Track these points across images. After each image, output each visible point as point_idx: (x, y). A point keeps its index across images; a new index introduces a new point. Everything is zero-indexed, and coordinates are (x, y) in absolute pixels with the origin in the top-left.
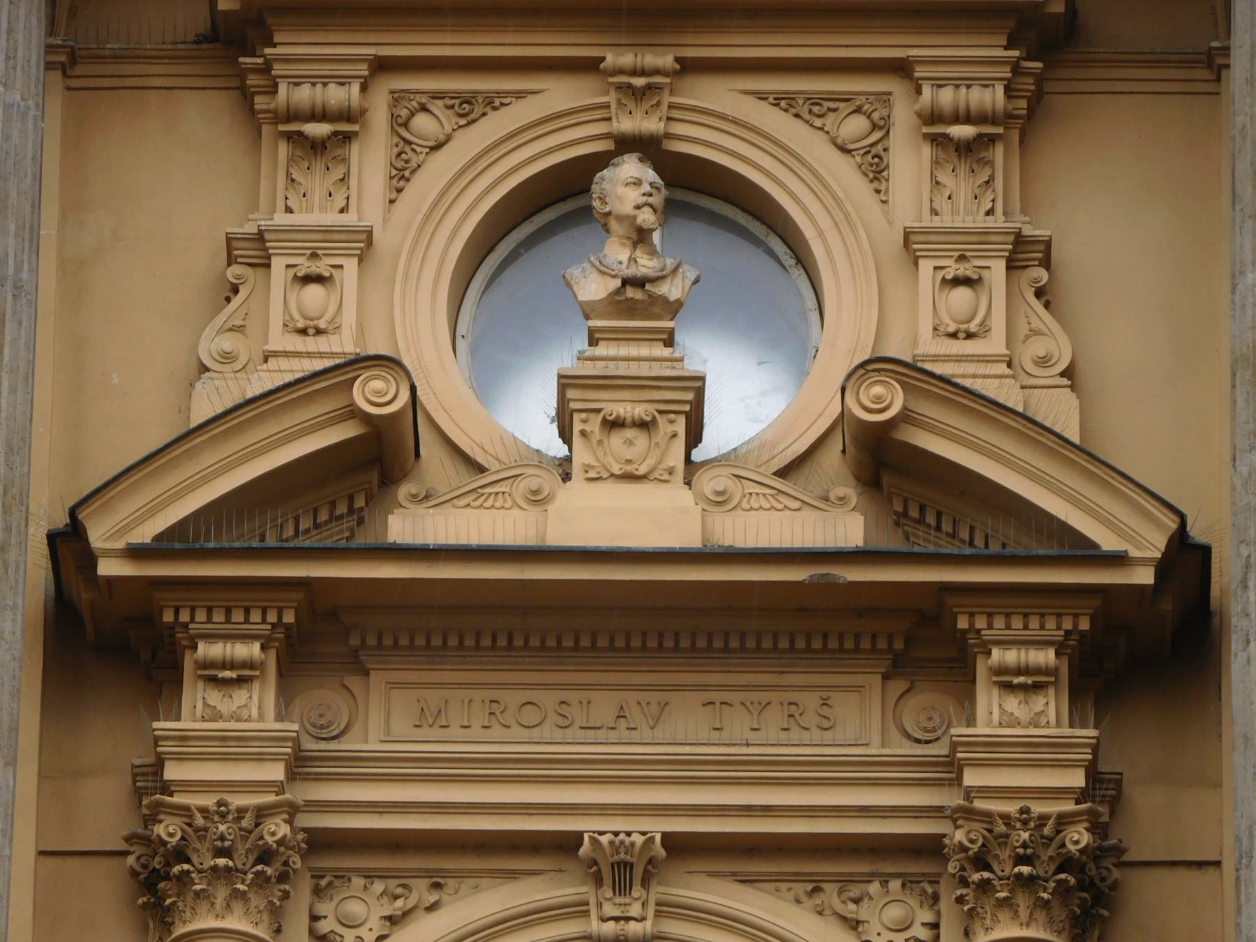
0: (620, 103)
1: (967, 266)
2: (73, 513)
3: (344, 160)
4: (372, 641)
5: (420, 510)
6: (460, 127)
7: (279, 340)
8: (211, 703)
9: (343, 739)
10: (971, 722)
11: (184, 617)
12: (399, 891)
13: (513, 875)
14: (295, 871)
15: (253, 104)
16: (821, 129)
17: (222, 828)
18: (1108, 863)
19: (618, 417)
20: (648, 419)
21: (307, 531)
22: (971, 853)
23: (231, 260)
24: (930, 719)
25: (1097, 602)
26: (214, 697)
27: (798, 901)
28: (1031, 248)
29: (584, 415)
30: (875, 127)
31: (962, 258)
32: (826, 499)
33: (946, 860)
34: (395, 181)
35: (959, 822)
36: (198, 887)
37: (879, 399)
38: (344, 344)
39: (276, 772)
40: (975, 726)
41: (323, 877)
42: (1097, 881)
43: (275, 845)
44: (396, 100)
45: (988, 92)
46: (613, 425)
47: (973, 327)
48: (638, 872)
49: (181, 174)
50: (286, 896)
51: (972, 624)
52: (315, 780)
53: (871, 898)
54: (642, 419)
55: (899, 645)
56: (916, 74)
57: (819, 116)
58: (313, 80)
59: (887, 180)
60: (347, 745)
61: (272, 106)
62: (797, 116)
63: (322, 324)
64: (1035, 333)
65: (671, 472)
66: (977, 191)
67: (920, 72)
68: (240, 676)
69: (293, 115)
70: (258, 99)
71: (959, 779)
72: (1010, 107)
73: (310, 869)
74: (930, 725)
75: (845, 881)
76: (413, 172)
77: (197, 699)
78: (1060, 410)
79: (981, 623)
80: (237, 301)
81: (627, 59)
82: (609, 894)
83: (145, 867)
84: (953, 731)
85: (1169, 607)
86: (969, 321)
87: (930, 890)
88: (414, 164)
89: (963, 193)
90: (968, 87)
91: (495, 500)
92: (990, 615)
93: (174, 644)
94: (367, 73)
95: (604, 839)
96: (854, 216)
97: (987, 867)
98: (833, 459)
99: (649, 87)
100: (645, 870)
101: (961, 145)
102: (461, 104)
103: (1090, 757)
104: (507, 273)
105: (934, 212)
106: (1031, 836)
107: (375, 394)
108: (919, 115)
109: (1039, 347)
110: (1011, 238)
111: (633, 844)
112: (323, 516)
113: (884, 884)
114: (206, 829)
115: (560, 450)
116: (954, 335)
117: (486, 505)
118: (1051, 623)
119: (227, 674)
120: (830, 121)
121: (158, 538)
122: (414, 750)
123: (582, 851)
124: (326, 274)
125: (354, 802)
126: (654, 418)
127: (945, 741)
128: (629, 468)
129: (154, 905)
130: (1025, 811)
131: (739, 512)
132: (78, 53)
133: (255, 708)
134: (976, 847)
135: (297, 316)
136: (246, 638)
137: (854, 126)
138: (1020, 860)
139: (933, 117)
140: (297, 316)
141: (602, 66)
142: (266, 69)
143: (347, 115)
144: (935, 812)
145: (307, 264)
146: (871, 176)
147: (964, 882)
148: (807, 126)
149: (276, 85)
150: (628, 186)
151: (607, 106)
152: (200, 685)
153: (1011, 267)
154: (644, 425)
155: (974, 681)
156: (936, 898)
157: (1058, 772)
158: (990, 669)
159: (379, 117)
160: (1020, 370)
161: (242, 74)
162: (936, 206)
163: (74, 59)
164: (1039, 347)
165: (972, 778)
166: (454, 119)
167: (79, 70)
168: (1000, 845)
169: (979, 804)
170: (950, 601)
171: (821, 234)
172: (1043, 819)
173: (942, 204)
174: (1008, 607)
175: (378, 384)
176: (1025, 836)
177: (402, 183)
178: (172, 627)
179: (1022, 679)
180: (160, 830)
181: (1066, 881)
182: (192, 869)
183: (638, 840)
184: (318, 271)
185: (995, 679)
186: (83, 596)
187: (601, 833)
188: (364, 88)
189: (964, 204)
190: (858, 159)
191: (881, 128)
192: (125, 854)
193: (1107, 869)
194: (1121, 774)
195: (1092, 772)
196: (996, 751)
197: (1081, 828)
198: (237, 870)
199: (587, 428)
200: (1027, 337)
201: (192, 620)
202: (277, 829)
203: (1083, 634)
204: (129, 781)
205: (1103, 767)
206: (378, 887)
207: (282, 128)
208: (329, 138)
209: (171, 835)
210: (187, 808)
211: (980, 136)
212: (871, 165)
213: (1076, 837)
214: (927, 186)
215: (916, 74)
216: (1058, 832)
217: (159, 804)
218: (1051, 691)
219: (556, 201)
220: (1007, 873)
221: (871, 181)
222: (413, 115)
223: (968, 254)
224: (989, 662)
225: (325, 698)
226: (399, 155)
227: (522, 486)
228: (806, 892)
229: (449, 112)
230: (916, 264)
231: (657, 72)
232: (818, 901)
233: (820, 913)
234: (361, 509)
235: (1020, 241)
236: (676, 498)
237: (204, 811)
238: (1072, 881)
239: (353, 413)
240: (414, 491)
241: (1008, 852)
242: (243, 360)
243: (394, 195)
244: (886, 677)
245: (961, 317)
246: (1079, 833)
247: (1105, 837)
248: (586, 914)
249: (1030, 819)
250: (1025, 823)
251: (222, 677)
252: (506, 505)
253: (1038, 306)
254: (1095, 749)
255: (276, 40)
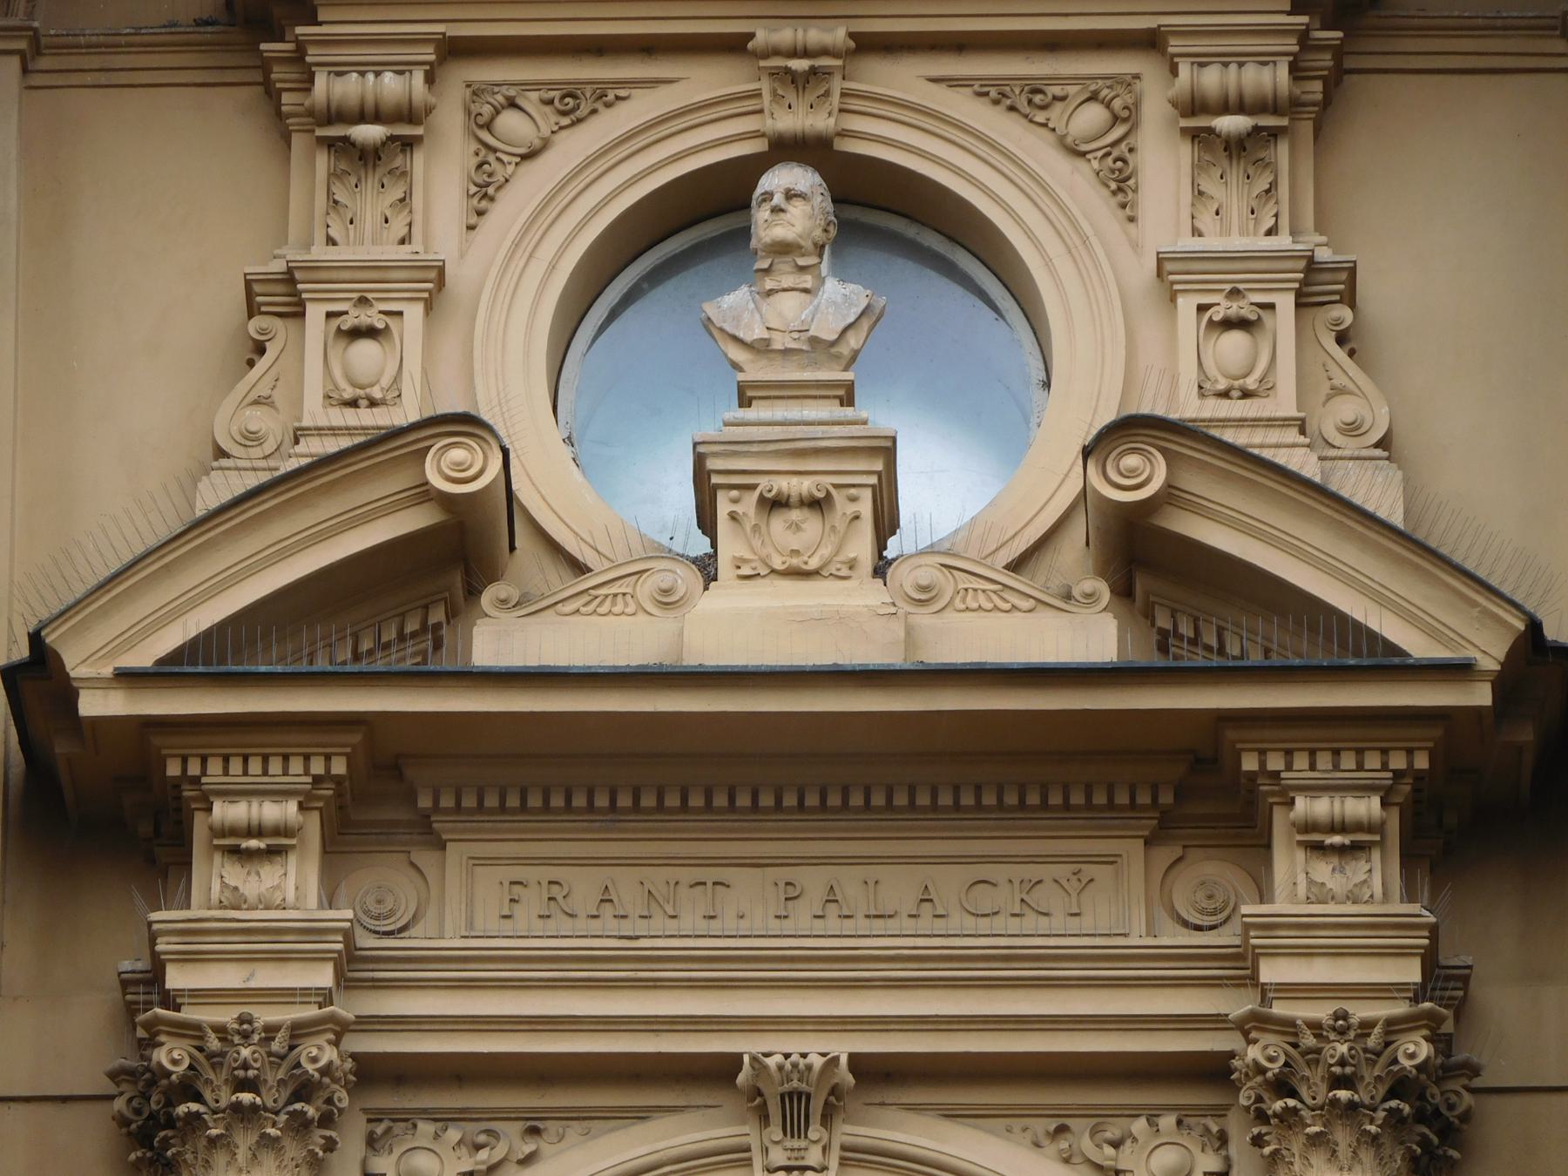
0: (776, 97)
1: (1241, 303)
2: (35, 639)
3: (404, 174)
4: (447, 801)
5: (506, 617)
6: (561, 128)
7: (315, 412)
8: (232, 883)
9: (412, 932)
10: (1264, 895)
11: (194, 769)
12: (482, 1138)
13: (641, 1115)
14: (341, 1111)
15: (279, 105)
16: (1045, 125)
17: (245, 1052)
18: (1455, 1085)
19: (779, 493)
20: (821, 495)
21: (370, 652)
22: (1269, 1074)
23: (252, 310)
24: (1210, 897)
25: (1437, 732)
26: (234, 874)
27: (1037, 1145)
28: (1327, 277)
29: (734, 493)
30: (1116, 119)
31: (1235, 293)
32: (1068, 597)
33: (1235, 1088)
34: (475, 201)
35: (1253, 1035)
36: (214, 1132)
37: (1132, 473)
38: (407, 412)
39: (323, 977)
40: (1271, 901)
41: (380, 1120)
42: (1444, 1111)
43: (317, 1075)
44: (474, 93)
45: (1266, 73)
46: (775, 504)
47: (1251, 383)
48: (817, 1107)
49: (181, 198)
50: (330, 1146)
51: (1263, 764)
52: (374, 987)
53: (1135, 1140)
54: (812, 496)
55: (1166, 798)
56: (1171, 50)
57: (1043, 108)
58: (362, 68)
59: (1135, 191)
60: (414, 941)
61: (307, 103)
62: (1012, 108)
63: (377, 393)
64: (1338, 391)
65: (852, 564)
66: (1254, 204)
67: (1175, 46)
68: (271, 846)
69: (336, 115)
70: (286, 98)
71: (1253, 979)
72: (1298, 92)
73: (365, 1111)
74: (1211, 905)
75: (1100, 1115)
76: (499, 188)
77: (214, 879)
78: (1377, 490)
79: (1275, 763)
80: (262, 364)
81: (785, 35)
82: (777, 1134)
83: (138, 1112)
84: (1245, 909)
85: (1531, 737)
86: (1245, 376)
87: (1215, 1129)
88: (499, 178)
89: (1235, 207)
90: (378, 74)
91: (614, 604)
92: (1289, 753)
93: (178, 810)
94: (433, 57)
95: (771, 1062)
96: (1093, 240)
97: (1293, 1094)
98: (1073, 554)
99: (813, 71)
100: (826, 1103)
101: (1232, 143)
102: (563, 97)
103: (1426, 941)
104: (629, 313)
105: (1197, 232)
106: (1350, 1049)
107: (453, 467)
108: (1174, 104)
109: (1347, 410)
110: (1302, 264)
111: (809, 1068)
112: (390, 634)
113: (1151, 1120)
114: (222, 1054)
115: (701, 545)
116: (1225, 394)
117: (600, 610)
118: (1372, 761)
119: (254, 843)
120: (1056, 114)
121: (161, 662)
122: (506, 939)
123: (741, 1078)
124: (380, 325)
125: (428, 1015)
126: (828, 494)
127: (1235, 926)
128: (795, 561)
129: (152, 1162)
130: (1345, 1016)
131: (950, 616)
132: (43, 41)
133: (292, 887)
134: (1275, 1067)
135: (343, 384)
136: (280, 794)
137: (1092, 116)
138: (1337, 1082)
139: (1194, 105)
140: (343, 384)
141: (750, 45)
142: (298, 57)
143: (409, 114)
144: (1215, 1022)
145: (353, 312)
146: (1114, 186)
147: (1262, 1117)
148: (1024, 122)
149: (311, 80)
150: (792, 204)
151: (757, 95)
152: (217, 858)
153: (1303, 303)
154: (818, 504)
155: (1268, 846)
156: (1223, 1139)
157: (1389, 963)
158: (1294, 824)
159: (450, 119)
160: (1320, 440)
161: (265, 66)
162: (1198, 224)
163: (37, 48)
164: (1347, 410)
165: (1270, 972)
166: (554, 118)
167: (44, 63)
168: (1308, 1063)
169: (1279, 1009)
170: (157, 741)
171: (1048, 262)
172: (1366, 1025)
173: (1206, 221)
174: (1262, 741)
175: (457, 454)
176: (1343, 1048)
177: (484, 204)
178: (176, 784)
179: (1337, 839)
180: (161, 1056)
181: (1399, 1110)
182: (202, 1109)
183: (817, 1062)
184: (369, 320)
185: (1299, 838)
186: (62, 748)
187: (767, 1055)
188: (430, 79)
189: (1236, 224)
190: (1095, 164)
191: (1125, 120)
192: (111, 1098)
193: (1457, 1093)
194: (1470, 967)
195: (1430, 961)
196: (1307, 937)
197: (1417, 1036)
198: (266, 1109)
199: (739, 508)
200: (1329, 398)
201: (204, 773)
202: (320, 1053)
203: (1419, 776)
204: (118, 994)
205: (1447, 958)
206: (453, 1134)
207: (320, 132)
208: (384, 144)
209: (175, 1062)
210: (197, 1027)
211: (1257, 129)
212: (1113, 171)
213: (1412, 1048)
214: (1187, 195)
215: (1171, 50)
216: (1387, 1044)
217: (158, 1020)
218: (1376, 855)
219: (696, 222)
220: (1319, 1101)
221: (1114, 193)
222: (498, 113)
223: (1241, 286)
224: (1292, 815)
225: (387, 881)
226: (480, 166)
227: (646, 589)
228: (1048, 1133)
229: (547, 109)
230: (1173, 300)
231: (825, 52)
232: (1064, 1145)
233: (1067, 1161)
234: (438, 626)
235: (1312, 266)
236: (865, 595)
237: (221, 1030)
238: (1406, 1109)
239: (424, 494)
240: (503, 596)
241: (1320, 1071)
242: (269, 447)
243: (473, 220)
244: (1148, 843)
245: (1235, 369)
246: (1416, 1044)
247: (1449, 1056)
248: (748, 1163)
249: (1349, 1028)
250: (246, 1036)
251: (242, 847)
252: (628, 610)
253: (1340, 354)
254: (1434, 930)
255: (320, 19)
